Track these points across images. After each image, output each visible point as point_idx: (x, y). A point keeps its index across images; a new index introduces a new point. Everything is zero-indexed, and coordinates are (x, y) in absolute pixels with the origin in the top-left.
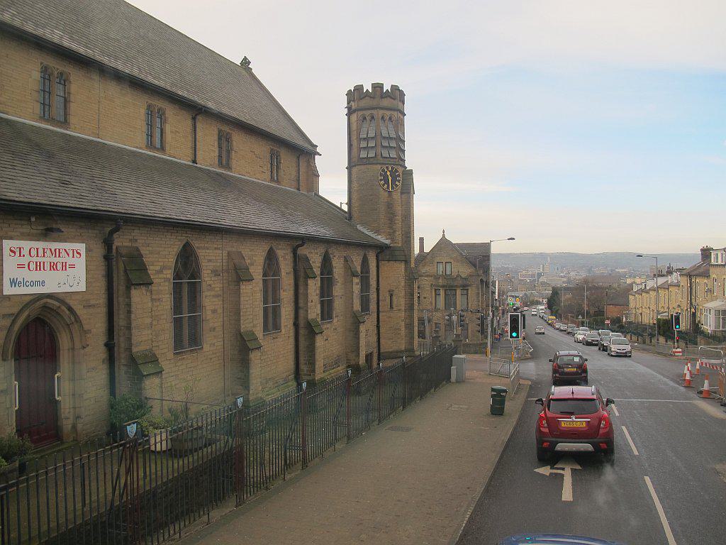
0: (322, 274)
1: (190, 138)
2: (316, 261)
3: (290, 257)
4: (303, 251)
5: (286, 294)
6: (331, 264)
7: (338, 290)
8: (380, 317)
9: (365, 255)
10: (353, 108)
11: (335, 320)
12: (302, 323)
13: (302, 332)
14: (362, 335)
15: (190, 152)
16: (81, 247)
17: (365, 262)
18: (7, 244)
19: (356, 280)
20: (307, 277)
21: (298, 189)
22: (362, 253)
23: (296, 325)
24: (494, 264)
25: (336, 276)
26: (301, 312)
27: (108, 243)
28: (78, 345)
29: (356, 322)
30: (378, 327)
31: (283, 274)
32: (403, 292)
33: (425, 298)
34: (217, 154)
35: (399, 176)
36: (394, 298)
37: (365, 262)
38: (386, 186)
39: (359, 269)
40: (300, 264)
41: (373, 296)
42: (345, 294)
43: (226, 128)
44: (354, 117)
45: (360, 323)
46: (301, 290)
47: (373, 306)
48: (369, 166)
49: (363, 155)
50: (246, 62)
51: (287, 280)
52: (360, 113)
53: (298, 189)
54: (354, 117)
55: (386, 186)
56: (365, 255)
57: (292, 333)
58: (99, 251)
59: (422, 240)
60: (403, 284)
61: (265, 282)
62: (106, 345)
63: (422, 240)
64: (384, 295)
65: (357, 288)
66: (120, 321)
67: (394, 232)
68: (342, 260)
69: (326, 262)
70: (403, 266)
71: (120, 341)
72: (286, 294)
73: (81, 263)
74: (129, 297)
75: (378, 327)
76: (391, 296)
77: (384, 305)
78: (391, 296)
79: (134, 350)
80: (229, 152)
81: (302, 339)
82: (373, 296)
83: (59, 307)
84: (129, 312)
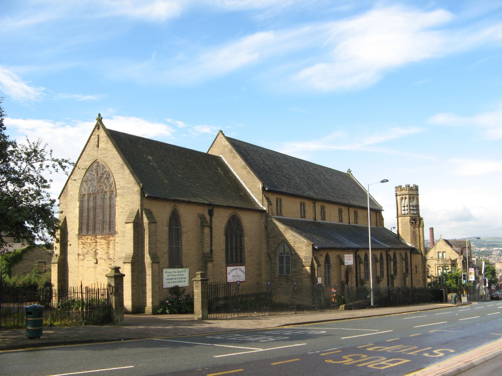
0: (364, 262)
1: (348, 216)
2: (391, 253)
3: (385, 255)
4: (389, 253)
5: (385, 266)
6: (396, 255)
7: (398, 265)
8: (412, 276)
9: (406, 252)
10: (398, 194)
11: (398, 275)
12: (389, 275)
13: (390, 278)
14: (407, 281)
15: (348, 220)
16: (352, 255)
17: (406, 255)
18: (345, 255)
19: (404, 262)
20: (360, 263)
21: (377, 226)
22: (405, 251)
23: (388, 276)
24: (124, 317)
25: (398, 260)
26: (389, 272)
27: (356, 253)
28: (352, 276)
29: (405, 276)
30: (412, 279)
31: (384, 260)
32: (421, 266)
33: (432, 271)
34: (354, 219)
35: (417, 220)
36: (417, 268)
37: (406, 255)
38: (412, 225)
39: (404, 257)
40: (388, 255)
41: (409, 268)
42: (401, 266)
43: (356, 209)
44: (399, 198)
45: (406, 276)
46: (389, 265)
47: (409, 272)
48: (405, 217)
49: (403, 212)
50: (349, 171)
51: (385, 262)
52: (401, 196)
53: (377, 226)
54: (399, 198)
55: (412, 225)
56: (406, 252)
57: (386, 278)
58: (354, 255)
59: (432, 229)
60: (421, 263)
61: (325, 266)
62: (356, 277)
63: (432, 229)
64: (414, 267)
65: (404, 264)
66: (358, 272)
67: (416, 242)
68: (399, 255)
69: (395, 255)
70: (420, 256)
71: (358, 276)
72: (385, 266)
73: (352, 258)
74: (360, 266)
75: (412, 279)
76: (416, 268)
77: (414, 272)
78: (416, 268)
79: (361, 278)
80: (357, 217)
81: (389, 280)
82: (409, 268)
83: (84, 293)
84: (360, 269)
